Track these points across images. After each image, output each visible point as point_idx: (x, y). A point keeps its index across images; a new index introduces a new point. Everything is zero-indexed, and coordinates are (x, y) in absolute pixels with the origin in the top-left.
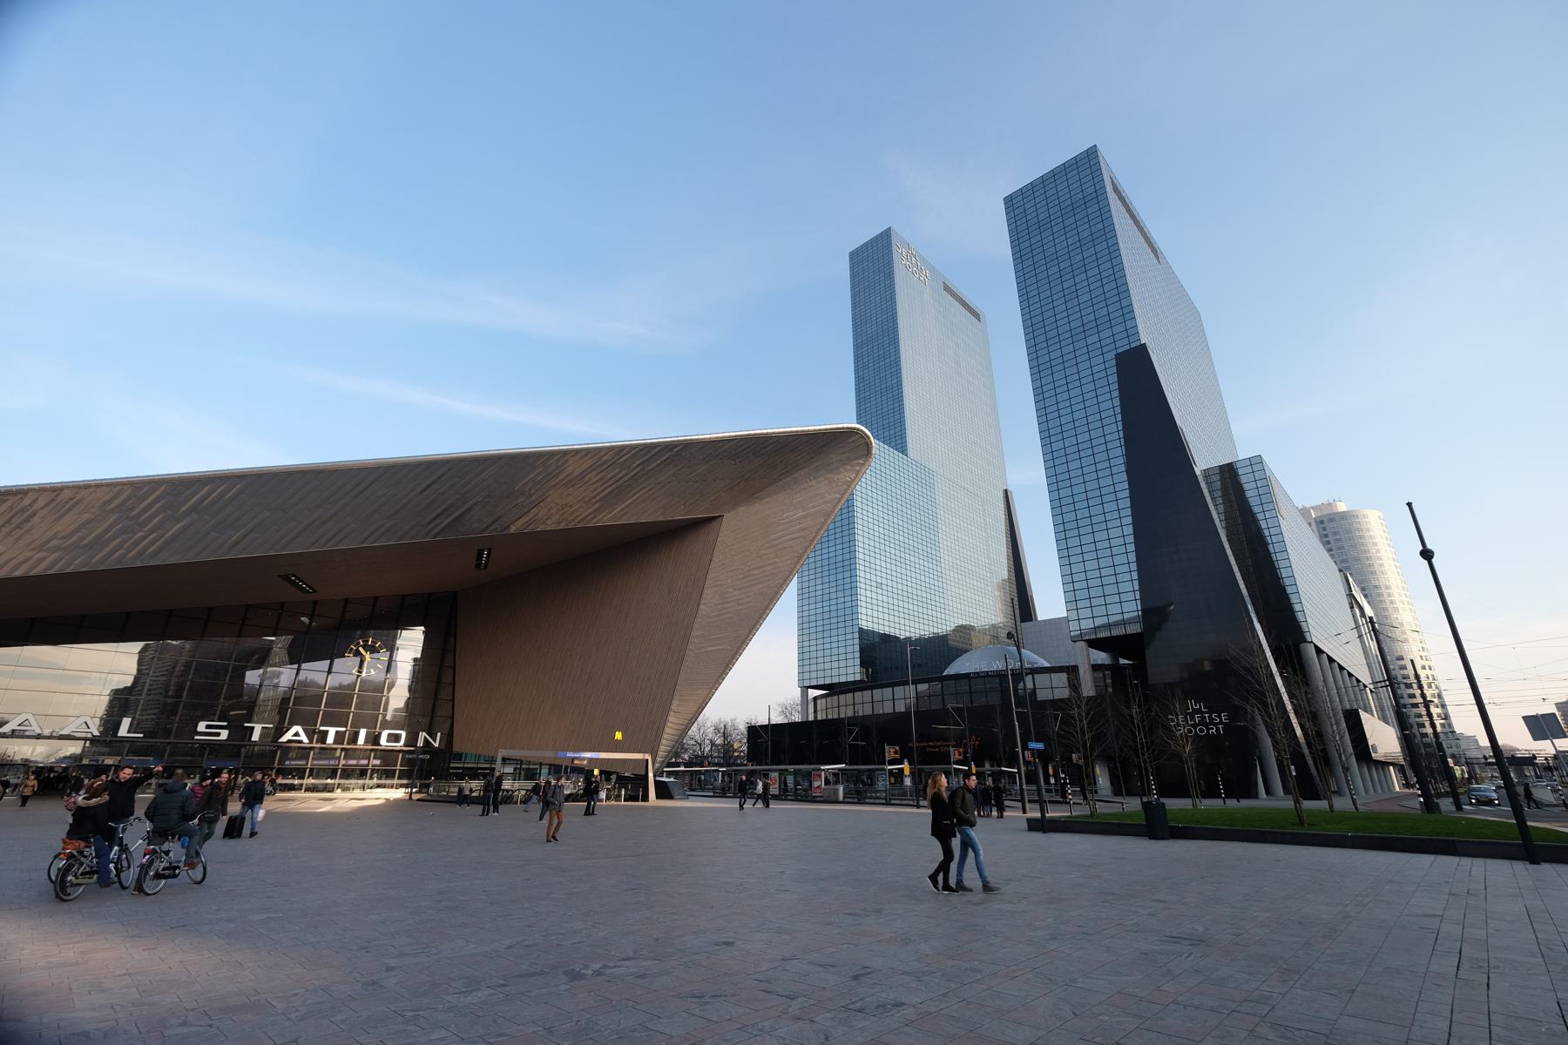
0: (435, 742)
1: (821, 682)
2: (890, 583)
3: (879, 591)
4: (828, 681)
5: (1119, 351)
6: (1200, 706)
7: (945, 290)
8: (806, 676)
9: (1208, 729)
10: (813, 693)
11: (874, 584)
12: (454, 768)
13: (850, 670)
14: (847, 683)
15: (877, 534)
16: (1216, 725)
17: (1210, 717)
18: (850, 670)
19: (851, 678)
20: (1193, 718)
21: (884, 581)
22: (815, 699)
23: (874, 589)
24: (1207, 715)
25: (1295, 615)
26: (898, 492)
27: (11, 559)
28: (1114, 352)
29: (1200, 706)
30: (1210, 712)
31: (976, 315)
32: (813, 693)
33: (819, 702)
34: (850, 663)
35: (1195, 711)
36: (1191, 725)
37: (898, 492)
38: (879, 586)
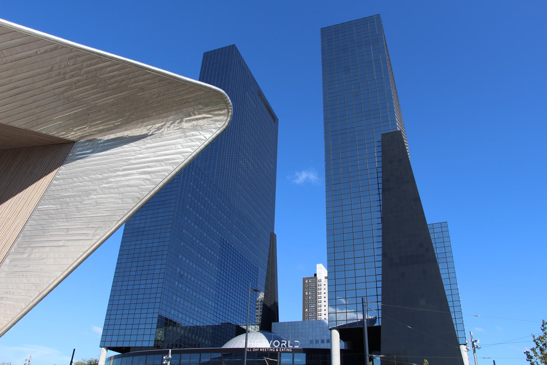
1: (120, 345)
4: (126, 345)
8: (109, 338)
13: (147, 338)
18: (147, 338)
19: (145, 344)
34: (149, 321)
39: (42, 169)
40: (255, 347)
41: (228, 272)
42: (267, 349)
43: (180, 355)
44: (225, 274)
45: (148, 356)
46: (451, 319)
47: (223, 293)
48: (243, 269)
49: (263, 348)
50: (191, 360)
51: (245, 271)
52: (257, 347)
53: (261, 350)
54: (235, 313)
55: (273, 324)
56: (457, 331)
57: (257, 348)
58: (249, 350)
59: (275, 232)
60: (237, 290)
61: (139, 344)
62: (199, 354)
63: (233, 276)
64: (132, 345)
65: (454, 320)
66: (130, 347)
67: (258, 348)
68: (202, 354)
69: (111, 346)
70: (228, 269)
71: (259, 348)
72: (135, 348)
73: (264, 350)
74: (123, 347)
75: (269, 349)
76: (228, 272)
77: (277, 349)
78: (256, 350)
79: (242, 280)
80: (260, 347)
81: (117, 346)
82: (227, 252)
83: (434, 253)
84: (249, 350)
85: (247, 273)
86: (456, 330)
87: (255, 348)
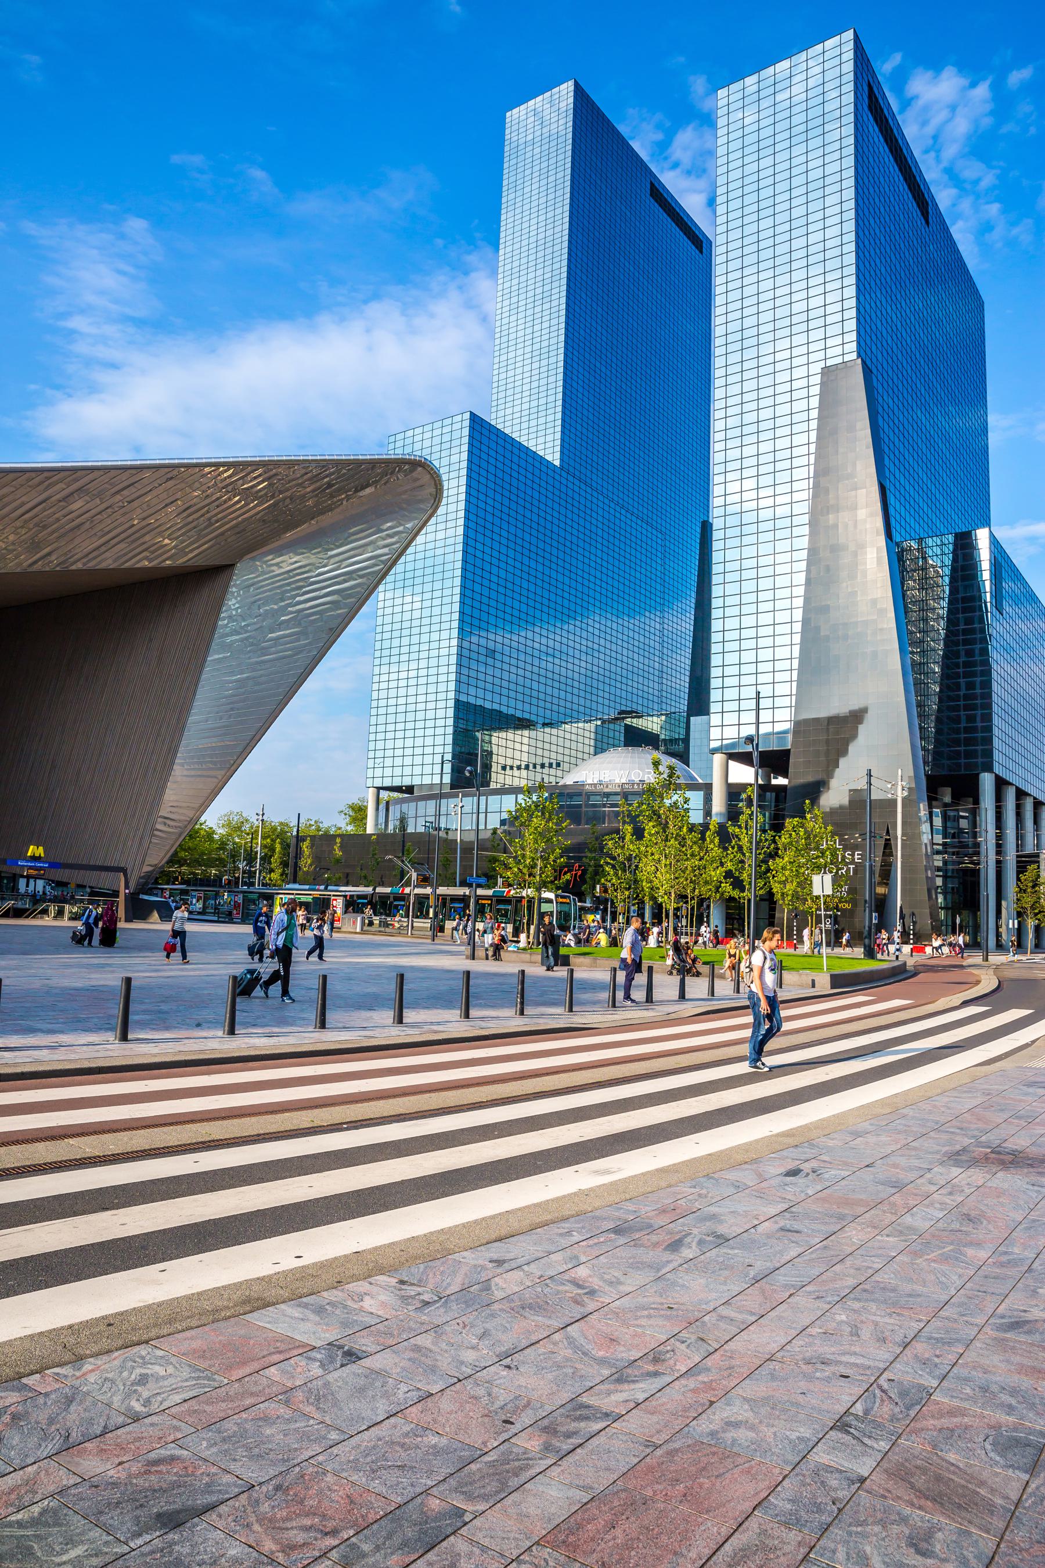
1: (397, 782)
3: (490, 661)
4: (407, 782)
5: (829, 363)
15: (494, 579)
23: (482, 658)
28: (822, 364)
31: (699, 242)
32: (384, 795)
33: (391, 808)
64: (416, 781)
69: (394, 784)
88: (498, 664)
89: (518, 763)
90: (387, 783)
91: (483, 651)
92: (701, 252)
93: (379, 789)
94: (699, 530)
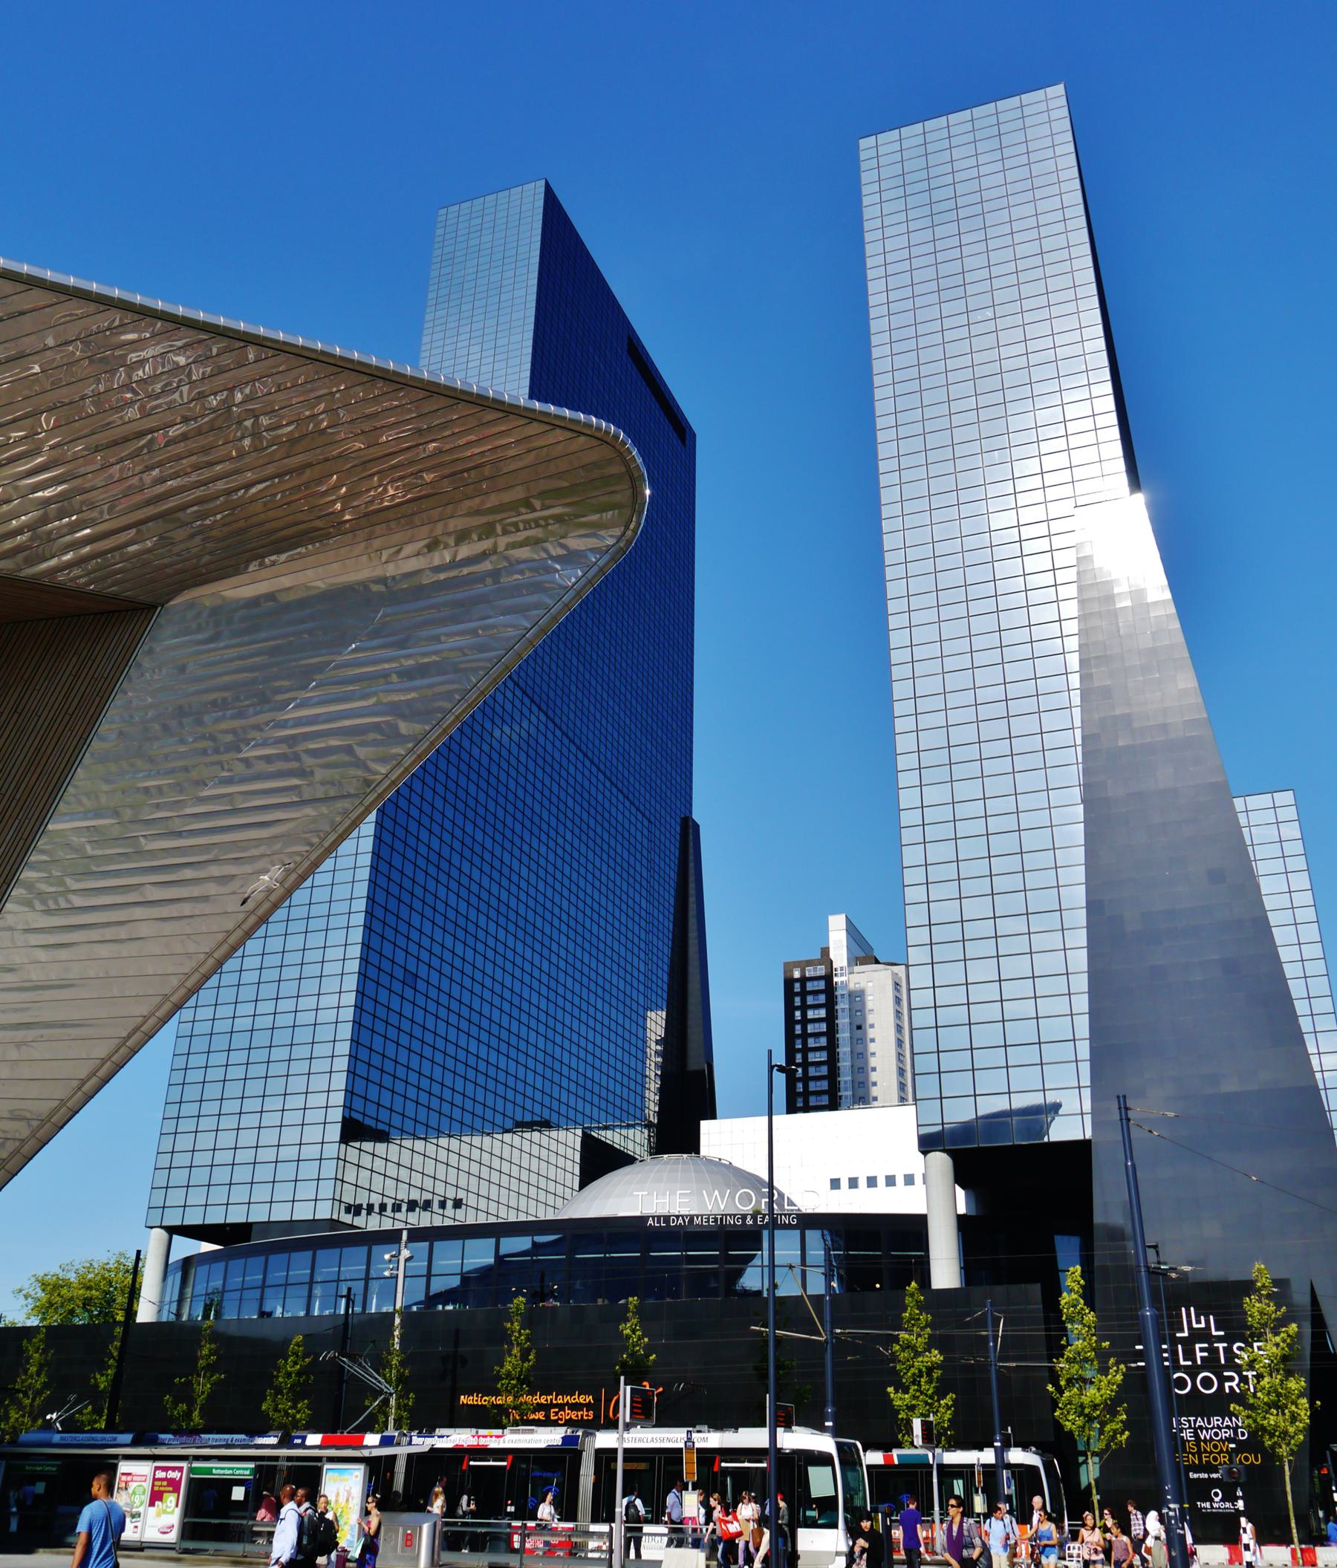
0: (820, 1335)
1: (215, 1217)
2: (434, 977)
3: (409, 993)
4: (237, 1216)
6: (1207, 1322)
7: (682, 432)
9: (1223, 1380)
10: (185, 1247)
11: (399, 973)
12: (53, 1466)
14: (291, 1225)
16: (1238, 1369)
17: (1228, 1351)
20: (1190, 1354)
21: (423, 971)
22: (187, 1263)
23: (397, 986)
24: (1221, 1346)
25: (952, 1131)
26: (453, 773)
27: (304, 522)
29: (1207, 1322)
30: (1230, 1339)
32: (185, 1247)
35: (1197, 1336)
36: (1186, 1369)
37: (453, 773)
38: (409, 979)
39: (46, 672)
40: (677, 1213)
41: (554, 959)
42: (716, 1220)
43: (366, 1248)
44: (545, 966)
45: (436, 1244)
46: (1307, 1056)
47: (542, 1029)
48: (602, 946)
49: (702, 1216)
50: (290, 1273)
51: (609, 952)
52: (682, 1213)
53: (697, 1221)
54: (491, 1085)
55: (705, 1125)
56: (1326, 1089)
57: (682, 1216)
58: (659, 1222)
59: (696, 816)
60: (477, 989)
61: (281, 1214)
62: (493, 1240)
63: (570, 970)
64: (258, 1215)
65: (1315, 1061)
66: (251, 1224)
67: (687, 1216)
68: (320, 1253)
70: (555, 947)
71: (692, 1217)
72: (268, 1226)
73: (708, 1222)
74: (225, 1225)
75: (722, 1219)
76: (554, 959)
77: (749, 1218)
78: (681, 1221)
79: (510, 955)
80: (692, 1213)
81: (185, 1223)
82: (549, 893)
83: (1311, 1068)
84: (659, 1222)
85: (609, 952)
86: (1248, 842)
87: (678, 1217)
88: (421, 1000)
89: (376, 1200)
90: (194, 1218)
91: (421, 986)
92: (684, 443)
93: (172, 1230)
94: (678, 829)
